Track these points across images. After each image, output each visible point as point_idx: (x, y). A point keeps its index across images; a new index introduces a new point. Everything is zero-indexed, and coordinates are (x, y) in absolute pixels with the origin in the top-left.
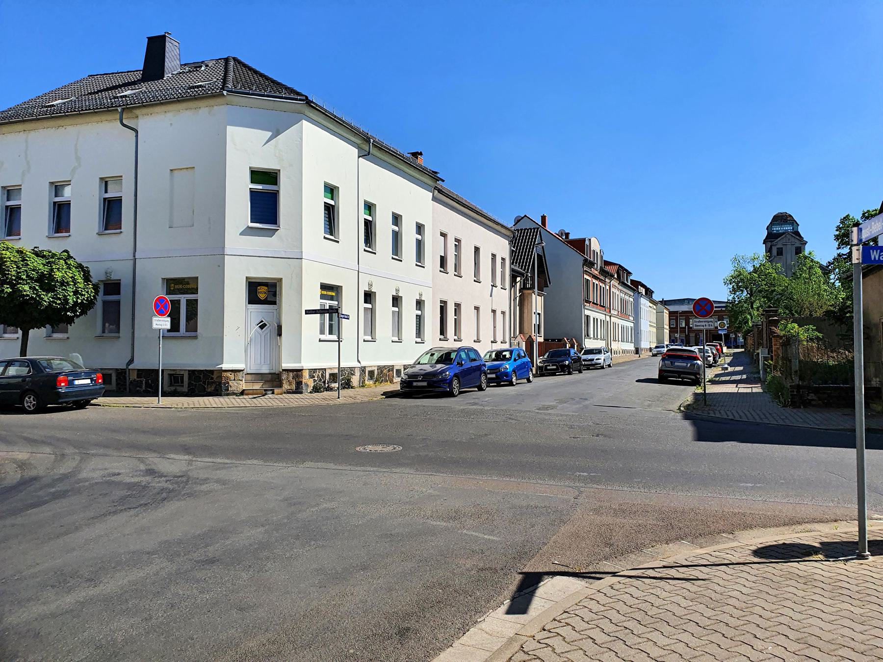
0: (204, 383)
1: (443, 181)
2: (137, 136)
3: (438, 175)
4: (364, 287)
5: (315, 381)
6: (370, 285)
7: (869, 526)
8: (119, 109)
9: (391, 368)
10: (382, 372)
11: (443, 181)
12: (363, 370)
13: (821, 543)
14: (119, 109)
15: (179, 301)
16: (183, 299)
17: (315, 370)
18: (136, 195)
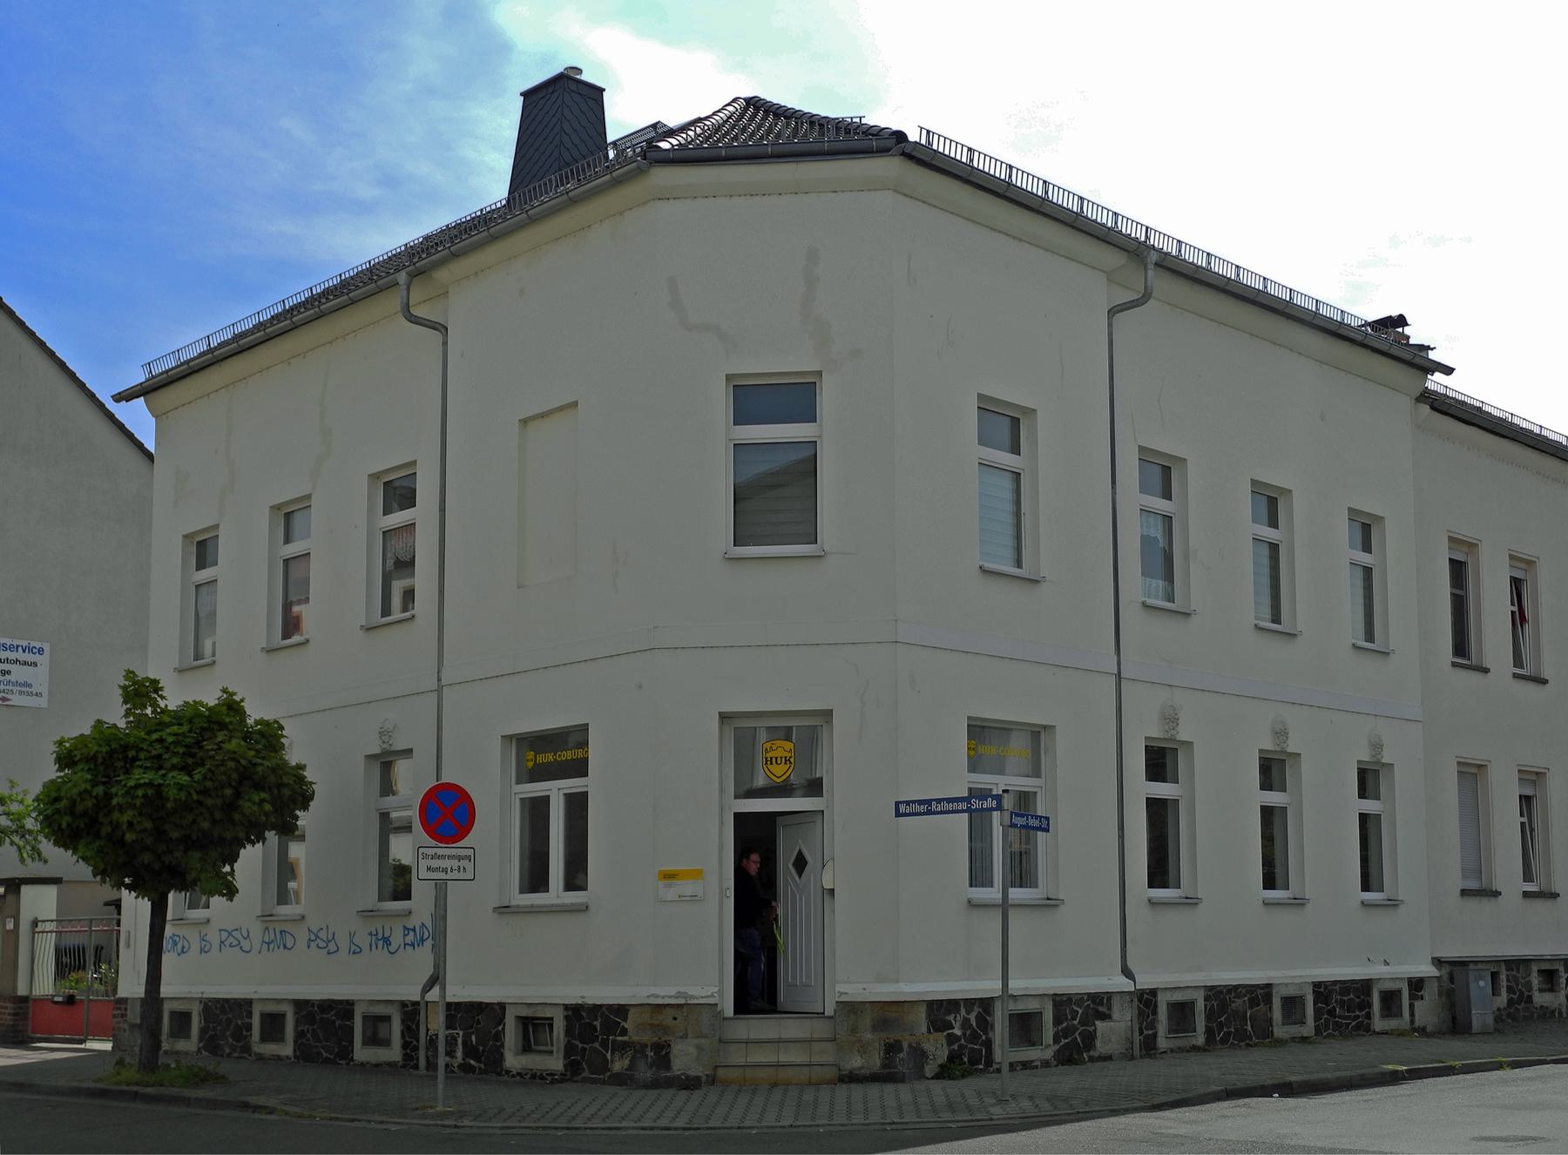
0: (604, 1044)
1: (1448, 371)
2: (445, 343)
3: (1432, 355)
4: (1143, 730)
5: (951, 1039)
6: (1171, 719)
7: (1012, 984)
8: (402, 277)
9: (1261, 994)
10: (1224, 1006)
11: (1448, 371)
12: (1146, 1000)
13: (1438, 962)
14: (402, 277)
15: (545, 801)
16: (556, 791)
17: (952, 1005)
18: (443, 510)
